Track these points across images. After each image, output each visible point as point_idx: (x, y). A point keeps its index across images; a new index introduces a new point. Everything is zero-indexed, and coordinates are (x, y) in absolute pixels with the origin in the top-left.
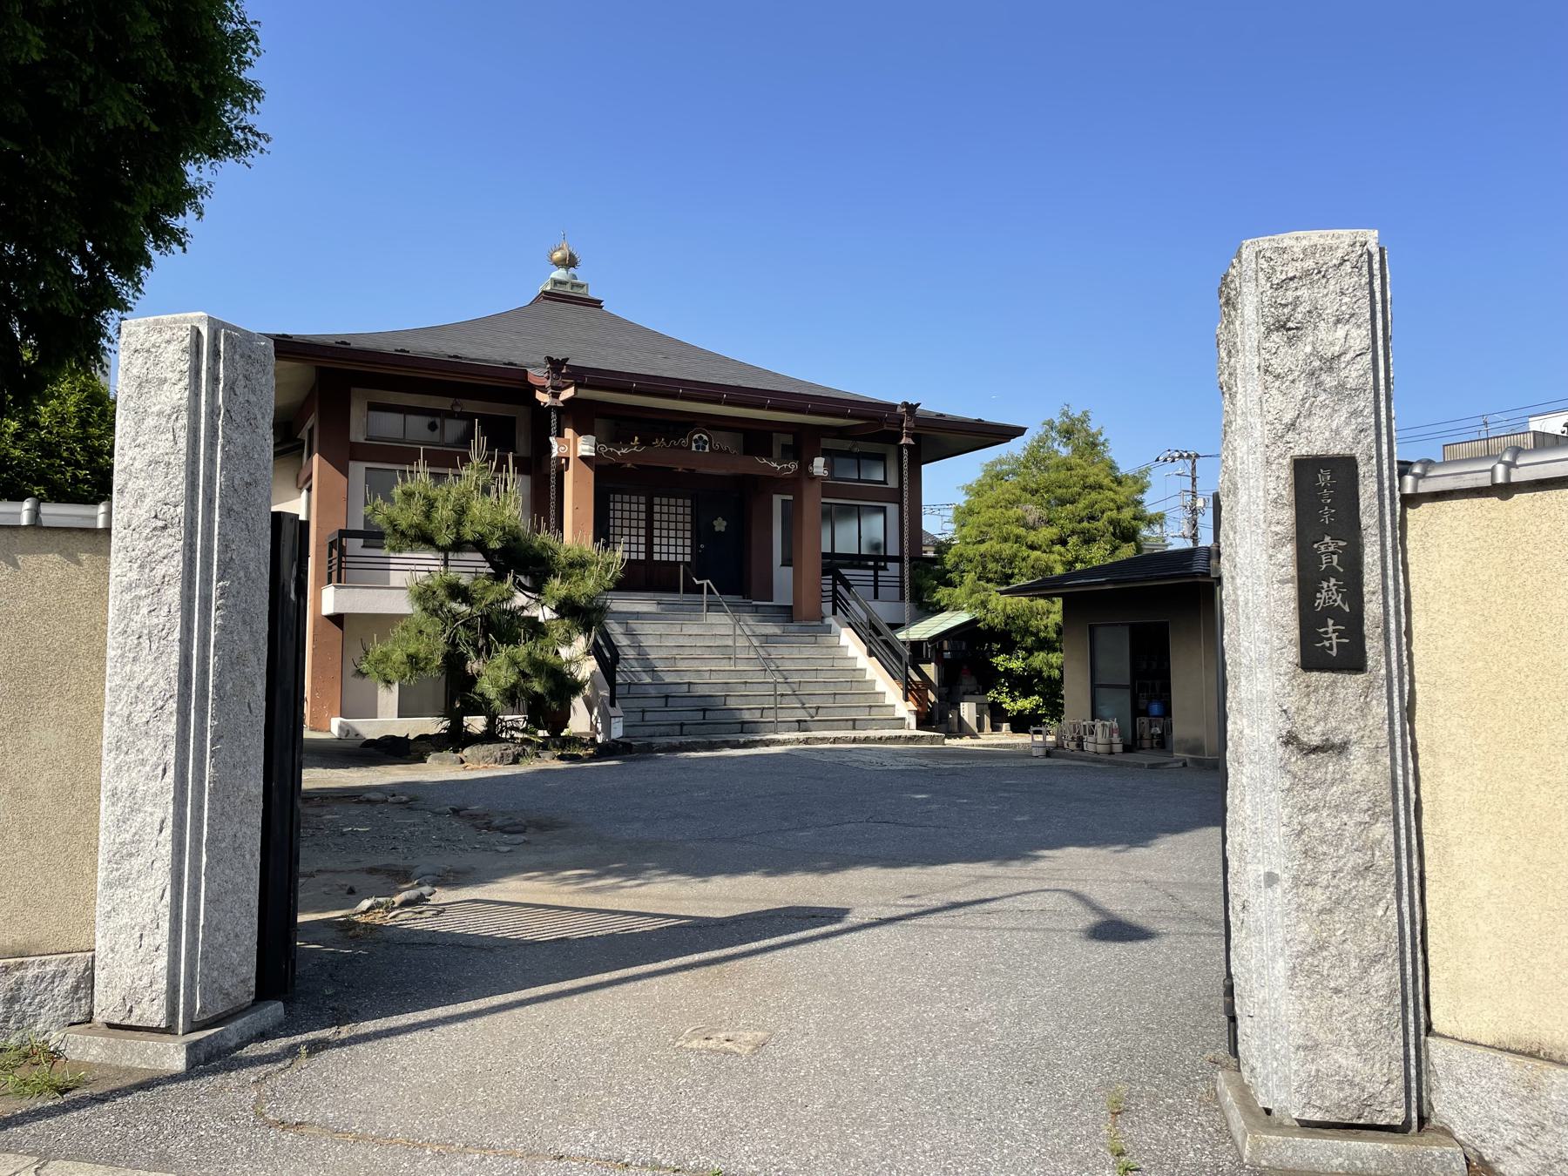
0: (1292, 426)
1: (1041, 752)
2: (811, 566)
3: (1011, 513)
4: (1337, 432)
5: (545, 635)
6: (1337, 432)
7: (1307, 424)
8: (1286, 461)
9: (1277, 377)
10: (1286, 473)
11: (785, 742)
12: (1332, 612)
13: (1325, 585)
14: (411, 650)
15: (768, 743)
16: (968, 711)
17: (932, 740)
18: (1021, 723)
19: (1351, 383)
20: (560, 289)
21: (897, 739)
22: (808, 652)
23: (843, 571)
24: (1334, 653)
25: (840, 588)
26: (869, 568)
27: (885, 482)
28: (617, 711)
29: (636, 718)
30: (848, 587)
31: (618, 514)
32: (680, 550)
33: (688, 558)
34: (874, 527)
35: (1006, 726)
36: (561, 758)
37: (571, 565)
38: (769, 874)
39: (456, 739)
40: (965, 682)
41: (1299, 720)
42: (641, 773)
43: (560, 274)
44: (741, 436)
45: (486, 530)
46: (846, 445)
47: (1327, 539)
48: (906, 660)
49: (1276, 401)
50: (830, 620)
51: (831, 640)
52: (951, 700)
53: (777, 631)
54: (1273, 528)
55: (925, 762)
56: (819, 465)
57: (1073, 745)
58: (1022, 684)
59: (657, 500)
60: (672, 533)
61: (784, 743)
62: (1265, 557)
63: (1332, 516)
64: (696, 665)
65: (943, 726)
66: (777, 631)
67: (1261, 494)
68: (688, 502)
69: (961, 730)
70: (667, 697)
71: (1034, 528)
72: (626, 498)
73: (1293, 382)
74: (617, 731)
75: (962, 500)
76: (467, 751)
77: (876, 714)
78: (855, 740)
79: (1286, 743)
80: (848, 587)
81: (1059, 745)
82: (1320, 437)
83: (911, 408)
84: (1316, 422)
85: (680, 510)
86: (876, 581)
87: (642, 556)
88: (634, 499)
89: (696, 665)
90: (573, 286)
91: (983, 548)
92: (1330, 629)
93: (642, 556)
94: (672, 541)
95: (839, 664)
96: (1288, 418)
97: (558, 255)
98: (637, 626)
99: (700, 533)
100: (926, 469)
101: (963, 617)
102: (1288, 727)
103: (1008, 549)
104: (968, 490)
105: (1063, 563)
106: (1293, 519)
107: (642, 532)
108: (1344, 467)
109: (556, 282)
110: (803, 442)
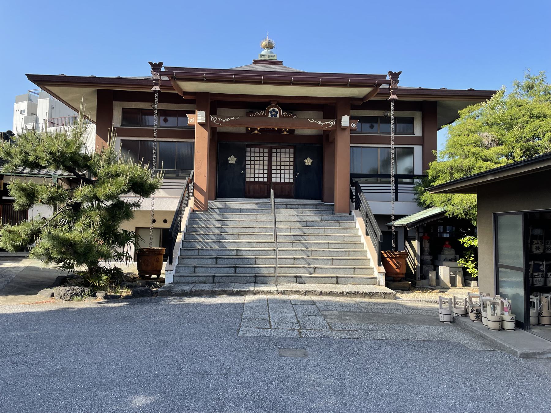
16: (444, 272)
20: (263, 58)
32: (287, 176)
33: (292, 180)
50: (353, 213)
51: (350, 224)
53: (318, 219)
56: (346, 120)
59: (274, 150)
60: (283, 167)
61: (267, 293)
66: (318, 219)
68: (292, 151)
69: (438, 285)
71: (486, 147)
72: (257, 150)
87: (266, 180)
88: (261, 150)
89: (253, 240)
90: (269, 56)
93: (266, 180)
94: (283, 172)
95: (348, 240)
99: (298, 166)
107: (266, 167)
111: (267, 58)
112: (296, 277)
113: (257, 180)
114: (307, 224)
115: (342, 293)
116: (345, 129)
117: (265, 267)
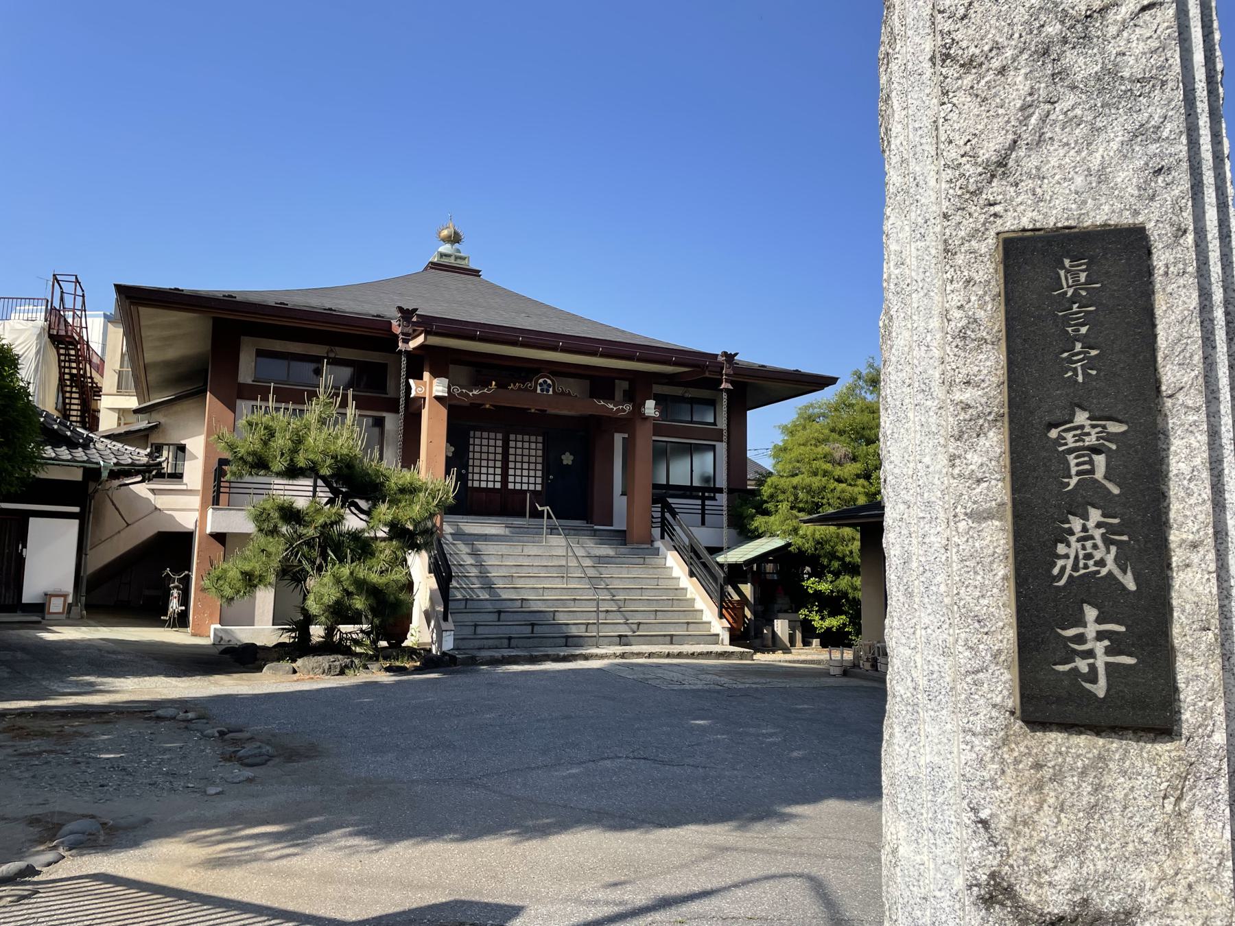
0: (999, 167)
1: (837, 671)
2: (643, 494)
3: (819, 449)
4: (1102, 176)
5: (372, 554)
6: (1102, 176)
7: (1031, 163)
8: (988, 245)
9: (969, 65)
10: (988, 272)
11: (601, 658)
12: (1092, 588)
13: (1076, 524)
14: (247, 568)
15: (586, 658)
16: (781, 627)
17: (742, 656)
18: (831, 639)
19: (1132, 67)
20: (445, 261)
21: (708, 655)
22: (637, 572)
23: (670, 500)
24: (1100, 688)
25: (667, 515)
26: (697, 498)
27: (715, 424)
28: (450, 625)
29: (467, 632)
30: (674, 514)
31: (477, 448)
32: (532, 480)
33: (539, 488)
34: (705, 464)
35: (816, 642)
36: (388, 669)
37: (402, 490)
38: (465, 838)
39: (299, 648)
40: (780, 601)
41: (1018, 847)
42: (459, 685)
43: (446, 248)
44: (588, 382)
45: (319, 458)
46: (678, 391)
47: (1081, 418)
48: (721, 581)
49: (967, 115)
50: (658, 544)
51: (657, 561)
52: (765, 616)
54: (958, 396)
55: (724, 680)
56: (650, 407)
57: (868, 666)
58: (831, 604)
60: (526, 466)
61: (602, 657)
62: (943, 460)
63: (1091, 363)
64: (530, 583)
65: (758, 642)
67: (935, 323)
68: (540, 439)
69: (774, 644)
70: (499, 612)
71: (840, 464)
72: (485, 434)
73: (1002, 71)
74: (448, 644)
75: (779, 439)
76: (300, 662)
77: (693, 631)
78: (668, 655)
79: (988, 901)
80: (674, 514)
81: (855, 665)
82: (1064, 189)
83: (730, 357)
84: (1054, 156)
85: (533, 446)
86: (703, 509)
87: (498, 485)
88: (492, 435)
89: (530, 583)
90: (457, 258)
91: (795, 480)
92: (1091, 630)
93: (498, 485)
94: (525, 473)
95: (663, 584)
96: (989, 151)
97: (445, 233)
98: (481, 546)
99: (550, 466)
100: (751, 415)
101: (777, 543)
102: (993, 861)
103: (817, 482)
104: (785, 429)
105: (867, 494)
106: (1002, 374)
107: (499, 464)
108: (1121, 254)
109: (442, 255)
110: (638, 386)
111: (452, 261)
112: (620, 636)
113: (483, 485)
114: (601, 560)
115: (693, 654)
116: (648, 418)
117: (575, 625)
